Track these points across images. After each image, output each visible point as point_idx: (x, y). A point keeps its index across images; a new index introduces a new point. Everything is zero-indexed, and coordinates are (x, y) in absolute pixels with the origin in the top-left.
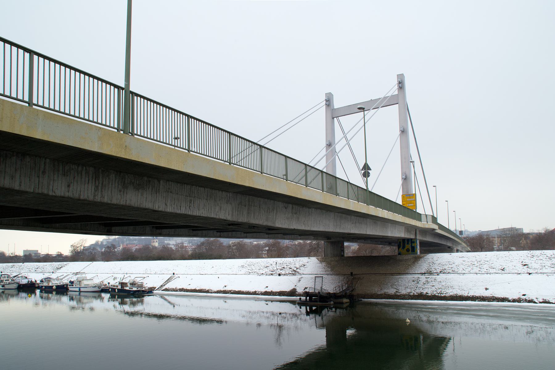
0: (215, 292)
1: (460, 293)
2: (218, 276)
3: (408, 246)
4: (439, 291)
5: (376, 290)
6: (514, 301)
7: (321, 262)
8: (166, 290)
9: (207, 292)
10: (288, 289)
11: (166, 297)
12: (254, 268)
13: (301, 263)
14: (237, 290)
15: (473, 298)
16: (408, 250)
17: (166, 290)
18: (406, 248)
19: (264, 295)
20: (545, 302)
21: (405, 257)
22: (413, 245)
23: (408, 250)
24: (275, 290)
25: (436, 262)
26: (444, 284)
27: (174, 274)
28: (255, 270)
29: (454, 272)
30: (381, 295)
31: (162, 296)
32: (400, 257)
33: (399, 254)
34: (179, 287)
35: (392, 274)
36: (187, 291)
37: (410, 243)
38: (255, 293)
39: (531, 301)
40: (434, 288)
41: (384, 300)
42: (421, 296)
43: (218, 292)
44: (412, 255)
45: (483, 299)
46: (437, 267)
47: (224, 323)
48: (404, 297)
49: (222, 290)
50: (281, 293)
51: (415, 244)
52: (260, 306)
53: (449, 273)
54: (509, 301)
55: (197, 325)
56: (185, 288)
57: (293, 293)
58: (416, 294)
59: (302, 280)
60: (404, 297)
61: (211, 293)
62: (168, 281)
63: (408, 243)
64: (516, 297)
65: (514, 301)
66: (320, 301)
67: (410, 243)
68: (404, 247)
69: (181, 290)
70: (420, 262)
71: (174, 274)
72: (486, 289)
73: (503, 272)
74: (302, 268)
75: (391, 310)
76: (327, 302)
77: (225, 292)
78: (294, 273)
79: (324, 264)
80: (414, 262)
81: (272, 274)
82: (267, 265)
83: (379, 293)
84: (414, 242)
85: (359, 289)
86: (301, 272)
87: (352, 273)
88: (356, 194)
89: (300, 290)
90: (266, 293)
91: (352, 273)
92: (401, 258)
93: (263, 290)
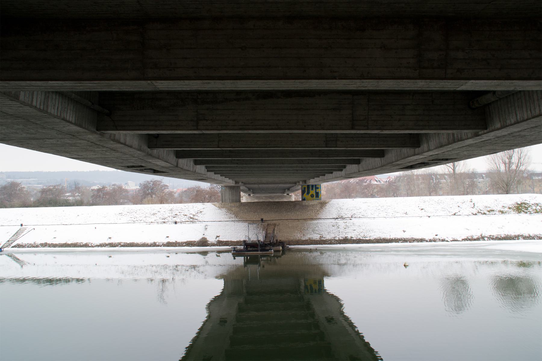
0: (98, 246)
1: (383, 236)
2: (95, 225)
3: (312, 192)
4: (362, 235)
5: (298, 236)
6: (430, 241)
7: (220, 208)
8: (19, 246)
9: (86, 245)
10: (197, 238)
11: (18, 256)
12: (138, 216)
13: (196, 210)
14: (63, 242)
15: (397, 240)
16: (312, 196)
17: (19, 246)
18: (310, 194)
19: (168, 246)
20: (454, 240)
21: (312, 203)
22: (317, 191)
23: (312, 196)
24: (180, 240)
25: (343, 207)
26: (364, 228)
27: (22, 225)
28: (141, 219)
29: (364, 217)
30: (307, 240)
31: (10, 255)
32: (305, 203)
33: (304, 199)
34: (39, 242)
35: (305, 220)
36: (55, 246)
37: (314, 189)
38: (154, 245)
39: (443, 240)
40: (356, 232)
41: (312, 246)
42: (346, 241)
43: (101, 245)
44: (318, 201)
45: (405, 241)
46: (346, 213)
47: (87, 282)
48: (331, 242)
49: (107, 242)
50: (189, 244)
51: (319, 190)
52: (159, 258)
53: (360, 217)
54: (427, 241)
55: (18, 285)
56: (49, 242)
57: (203, 243)
58: (341, 238)
59: (208, 227)
60: (331, 242)
61: (92, 247)
62: (17, 234)
63: (312, 189)
64: (431, 238)
65: (430, 241)
66: (261, 251)
67: (314, 189)
68: (308, 193)
69: (45, 245)
70: (327, 207)
71: (22, 225)
72: (404, 231)
73: (407, 215)
74: (199, 215)
75: (299, 255)
76: (268, 250)
77: (112, 245)
78: (192, 220)
79: (224, 210)
80: (321, 208)
81: (164, 222)
82: (154, 212)
83: (304, 239)
84: (318, 188)
85: (281, 236)
86: (200, 219)
87: (262, 220)
88: (515, 134)
89: (211, 239)
90: (169, 244)
91: (262, 220)
92: (307, 204)
93: (165, 241)
